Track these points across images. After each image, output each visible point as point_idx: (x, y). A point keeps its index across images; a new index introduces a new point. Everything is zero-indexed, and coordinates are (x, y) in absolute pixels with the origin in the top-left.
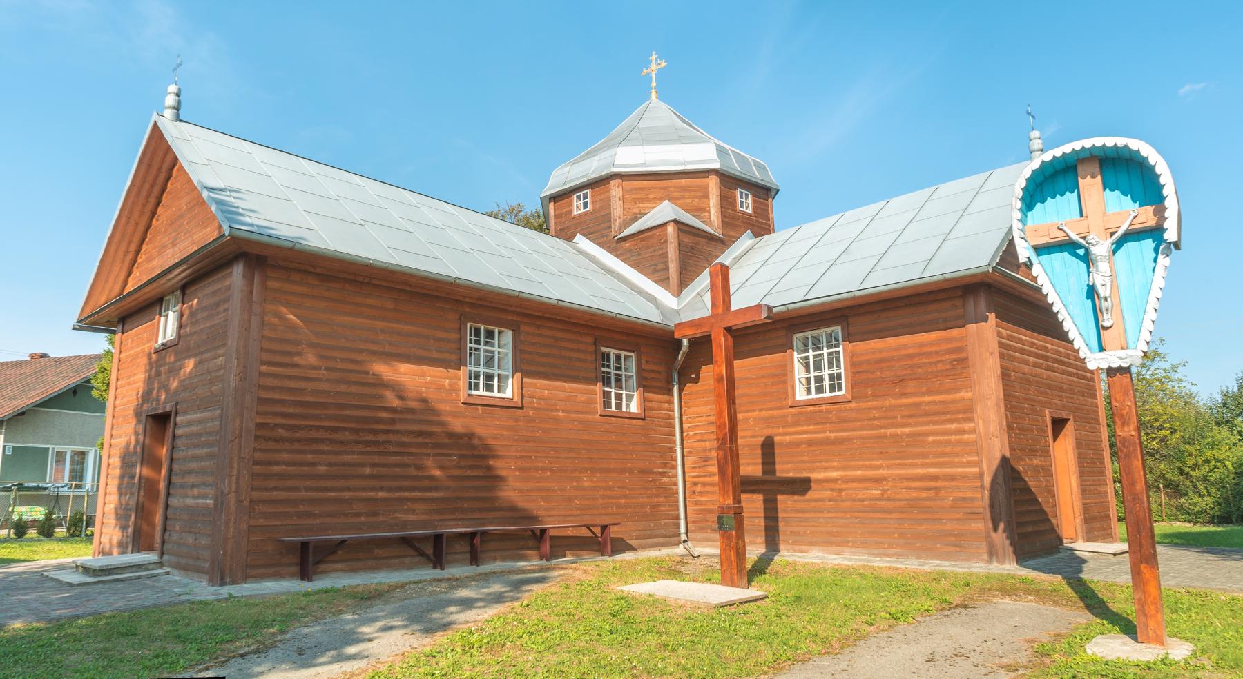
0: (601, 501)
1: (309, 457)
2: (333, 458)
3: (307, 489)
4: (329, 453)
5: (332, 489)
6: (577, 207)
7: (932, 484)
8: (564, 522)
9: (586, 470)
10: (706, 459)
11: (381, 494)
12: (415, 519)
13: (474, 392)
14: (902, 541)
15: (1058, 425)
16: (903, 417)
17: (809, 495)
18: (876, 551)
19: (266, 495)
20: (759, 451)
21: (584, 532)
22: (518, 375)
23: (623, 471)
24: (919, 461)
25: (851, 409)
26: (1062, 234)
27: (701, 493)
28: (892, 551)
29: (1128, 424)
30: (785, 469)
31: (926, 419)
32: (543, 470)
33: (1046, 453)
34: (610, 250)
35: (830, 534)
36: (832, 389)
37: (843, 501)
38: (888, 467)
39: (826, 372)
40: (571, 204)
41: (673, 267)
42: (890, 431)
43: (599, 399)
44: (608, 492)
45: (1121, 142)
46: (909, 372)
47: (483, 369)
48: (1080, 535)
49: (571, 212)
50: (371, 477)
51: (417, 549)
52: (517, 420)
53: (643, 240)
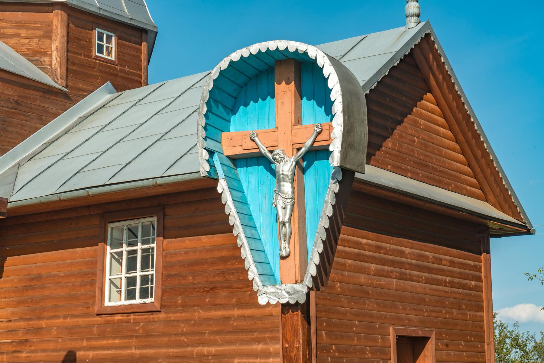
16: (212, 333)
31: (233, 337)
36: (142, 297)
39: (138, 274)
42: (196, 350)
45: (302, 47)
46: (221, 278)
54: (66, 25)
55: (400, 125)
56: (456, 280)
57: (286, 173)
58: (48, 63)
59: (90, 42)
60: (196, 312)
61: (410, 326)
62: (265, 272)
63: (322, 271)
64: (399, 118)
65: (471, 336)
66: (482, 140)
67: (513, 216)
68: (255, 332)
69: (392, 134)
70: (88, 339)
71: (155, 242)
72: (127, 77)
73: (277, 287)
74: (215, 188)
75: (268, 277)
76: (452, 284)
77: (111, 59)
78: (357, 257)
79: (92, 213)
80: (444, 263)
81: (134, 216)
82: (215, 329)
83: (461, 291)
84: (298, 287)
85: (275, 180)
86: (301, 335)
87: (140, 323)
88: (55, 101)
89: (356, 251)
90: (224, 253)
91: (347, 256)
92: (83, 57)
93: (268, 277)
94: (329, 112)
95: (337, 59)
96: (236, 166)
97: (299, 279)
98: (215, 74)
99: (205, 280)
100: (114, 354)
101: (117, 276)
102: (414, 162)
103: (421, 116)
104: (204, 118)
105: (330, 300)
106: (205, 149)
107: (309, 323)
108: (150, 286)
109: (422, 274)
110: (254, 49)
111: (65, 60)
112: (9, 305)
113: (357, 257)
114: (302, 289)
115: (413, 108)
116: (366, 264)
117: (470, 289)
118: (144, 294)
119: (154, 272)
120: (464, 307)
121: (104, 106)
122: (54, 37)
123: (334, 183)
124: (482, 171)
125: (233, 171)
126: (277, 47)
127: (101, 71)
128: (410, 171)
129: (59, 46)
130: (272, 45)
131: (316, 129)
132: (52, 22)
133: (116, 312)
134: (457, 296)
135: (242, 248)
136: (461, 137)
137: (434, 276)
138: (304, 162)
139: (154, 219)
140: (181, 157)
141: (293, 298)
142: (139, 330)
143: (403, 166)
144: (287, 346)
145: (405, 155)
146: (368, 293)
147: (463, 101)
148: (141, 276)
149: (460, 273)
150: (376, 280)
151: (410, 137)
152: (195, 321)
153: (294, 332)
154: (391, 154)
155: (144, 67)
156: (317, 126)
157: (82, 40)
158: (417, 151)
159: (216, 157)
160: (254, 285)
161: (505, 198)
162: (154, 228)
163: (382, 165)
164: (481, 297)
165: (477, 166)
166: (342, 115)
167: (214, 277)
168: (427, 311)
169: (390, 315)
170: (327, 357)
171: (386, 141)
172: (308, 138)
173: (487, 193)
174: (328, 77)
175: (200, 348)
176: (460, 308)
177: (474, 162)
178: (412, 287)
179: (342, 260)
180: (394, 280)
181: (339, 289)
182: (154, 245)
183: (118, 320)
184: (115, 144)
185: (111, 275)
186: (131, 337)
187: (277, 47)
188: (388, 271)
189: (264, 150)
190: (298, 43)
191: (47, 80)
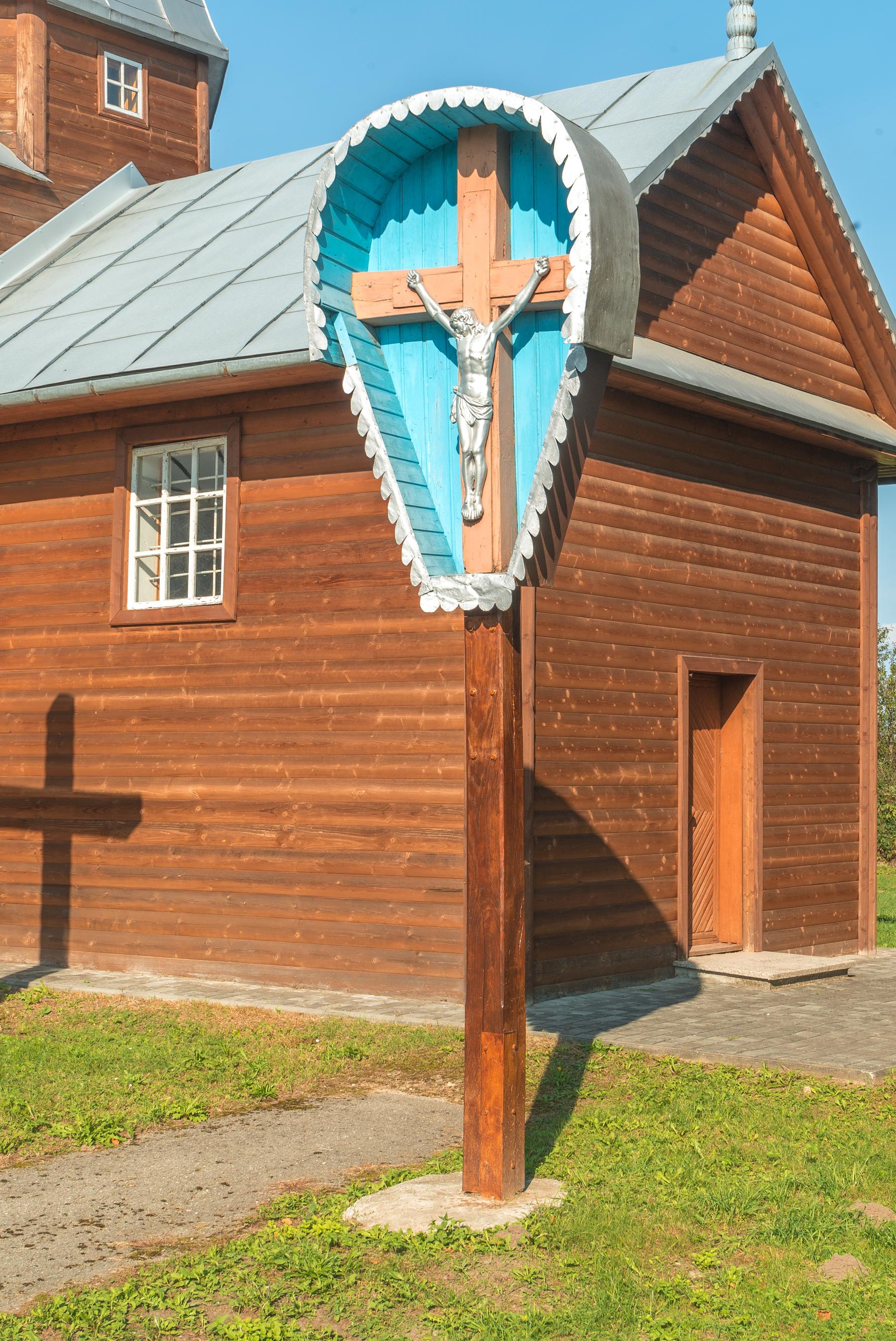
7: (375, 822)
15: (716, 694)
16: (334, 663)
17: (138, 836)
18: (256, 969)
20: (42, 728)
24: (354, 768)
26: (412, 298)
28: (288, 971)
29: (490, 736)
30: (93, 777)
31: (374, 671)
33: (665, 752)
35: (170, 928)
36: (199, 593)
37: (202, 852)
38: (297, 777)
39: (192, 547)
45: (512, 101)
46: (351, 559)
48: (750, 934)
54: (44, 43)
55: (709, 257)
56: (808, 566)
57: (476, 355)
58: (9, 123)
60: (303, 623)
61: (717, 654)
62: (435, 550)
63: (545, 549)
64: (708, 244)
65: (833, 673)
66: (870, 289)
68: (418, 662)
69: (692, 276)
70: (97, 673)
71: (225, 487)
72: (169, 153)
73: (457, 578)
74: (338, 381)
75: (440, 559)
76: (801, 574)
77: (135, 115)
78: (617, 521)
79: (100, 428)
80: (787, 532)
81: (183, 435)
82: (340, 656)
83: (817, 587)
84: (497, 579)
85: (456, 369)
86: (501, 671)
87: (196, 642)
88: (25, 202)
89: (616, 508)
90: (359, 510)
91: (598, 517)
92: (78, 112)
93: (440, 559)
94: (563, 234)
95: (583, 124)
96: (380, 340)
97: (499, 564)
98: (339, 153)
99: (322, 561)
100: (147, 701)
101: (153, 550)
102: (735, 333)
103: (751, 241)
104: (317, 244)
105: (562, 602)
106: (319, 305)
107: (517, 647)
108: (214, 571)
109: (743, 553)
110: (417, 104)
111: (43, 117)
113: (617, 521)
114: (505, 582)
115: (736, 224)
116: (635, 534)
117: (835, 583)
118: (204, 587)
119: (222, 546)
120: (822, 618)
121: (121, 212)
122: (20, 70)
123: (571, 377)
124: (869, 351)
125: (373, 350)
126: (463, 101)
127: (115, 141)
128: (725, 351)
129: (30, 89)
130: (453, 96)
131: (537, 268)
132: (15, 38)
133: (149, 621)
134: (810, 597)
135: (390, 503)
136: (829, 282)
137: (766, 558)
138: (513, 333)
139: (223, 441)
140: (275, 319)
141: (488, 601)
142: (194, 655)
143: (714, 341)
144: (475, 691)
145: (717, 319)
146: (637, 590)
147: (835, 211)
148: (198, 553)
149: (817, 553)
150: (653, 565)
151: (728, 283)
152: (301, 639)
153: (489, 665)
154: (689, 317)
155: (202, 133)
156: (540, 263)
157: (77, 76)
158: (741, 310)
159: (340, 321)
160: (413, 574)
162: (221, 456)
163: (671, 340)
164: (856, 599)
165: (859, 342)
166: (588, 240)
167: (340, 555)
168: (749, 625)
169: (678, 633)
170: (556, 711)
171: (681, 290)
172: (523, 286)
173: (877, 396)
174: (564, 163)
175: (311, 692)
176: (814, 620)
177: (852, 334)
178: (722, 578)
179: (587, 526)
180: (688, 566)
181: (581, 582)
182: (223, 493)
183: (153, 637)
184: (144, 291)
185: (138, 550)
186: (179, 669)
187: (463, 101)
188: (677, 548)
189: (435, 309)
190: (504, 92)
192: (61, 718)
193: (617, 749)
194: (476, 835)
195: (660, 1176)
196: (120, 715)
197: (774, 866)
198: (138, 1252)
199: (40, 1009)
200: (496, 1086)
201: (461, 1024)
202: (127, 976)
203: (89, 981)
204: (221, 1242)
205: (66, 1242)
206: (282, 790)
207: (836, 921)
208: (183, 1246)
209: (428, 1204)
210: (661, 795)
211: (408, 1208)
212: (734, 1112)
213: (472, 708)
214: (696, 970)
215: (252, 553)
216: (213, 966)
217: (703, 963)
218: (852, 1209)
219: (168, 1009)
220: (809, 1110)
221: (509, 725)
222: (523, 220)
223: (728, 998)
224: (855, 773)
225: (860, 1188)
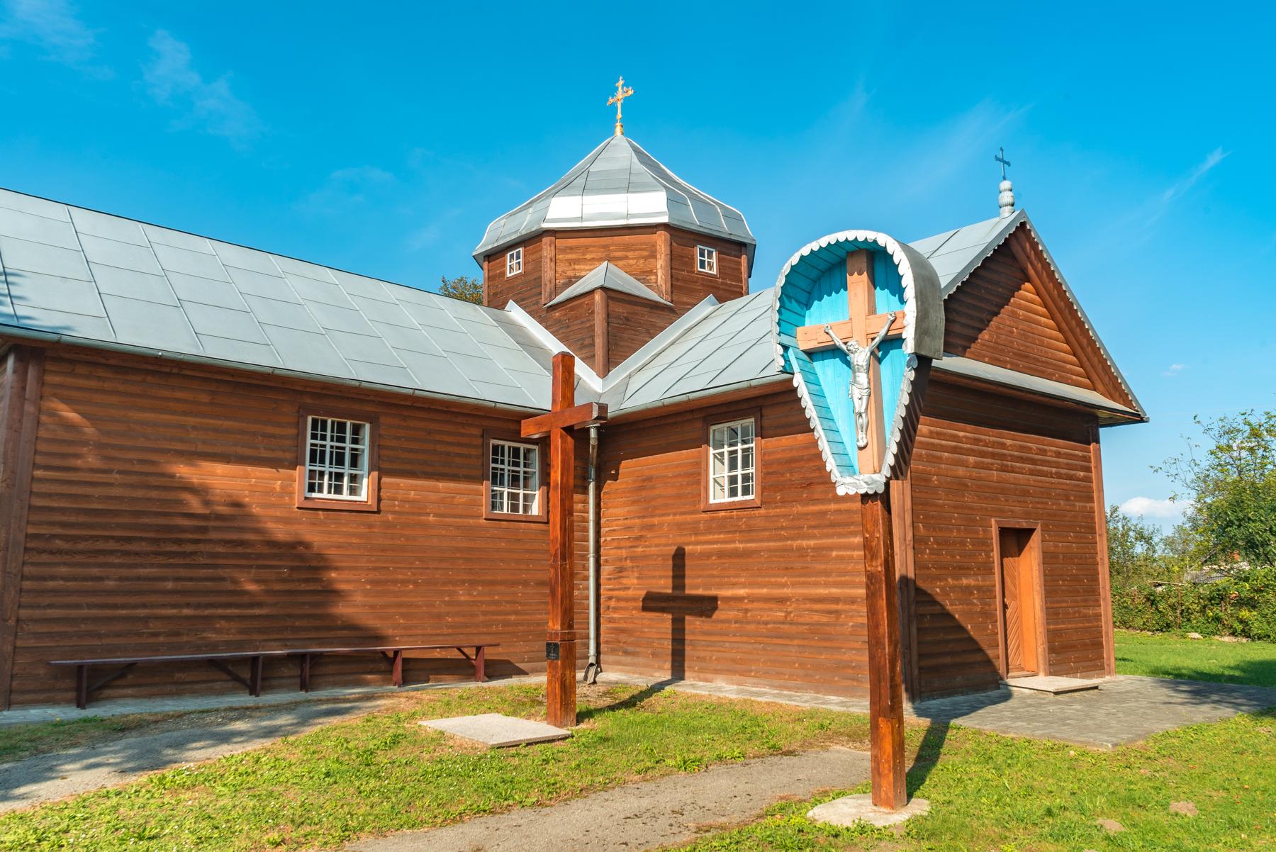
0: (481, 618)
1: (95, 571)
2: (124, 572)
3: (90, 606)
4: (121, 566)
5: (123, 606)
6: (513, 266)
7: (834, 607)
8: (429, 642)
9: (463, 582)
10: (621, 570)
11: (186, 612)
12: (223, 638)
13: (314, 495)
14: (802, 672)
15: (1014, 539)
16: (809, 527)
17: (716, 615)
18: (776, 682)
19: (38, 613)
21: (455, 654)
22: (375, 474)
23: (515, 583)
24: (822, 579)
25: (760, 516)
27: (615, 609)
28: (792, 683)
30: (695, 587)
31: (830, 531)
32: (404, 582)
34: (541, 321)
35: (734, 661)
37: (748, 623)
38: (794, 585)
39: (739, 472)
40: (504, 265)
41: (599, 341)
42: (796, 544)
43: (485, 501)
44: (493, 608)
45: (871, 235)
47: (347, 470)
48: (1042, 667)
49: (504, 273)
50: (174, 592)
51: (229, 673)
52: (370, 526)
53: (572, 309)
56: (1062, 471)
59: (692, 258)
65: (1081, 527)
67: (1125, 405)
72: (729, 288)
75: (847, 468)
76: (1059, 476)
78: (954, 450)
84: (876, 477)
93: (847, 468)
110: (823, 242)
112: (625, 504)
113: (954, 450)
114: (880, 479)
117: (1078, 479)
118: (746, 491)
130: (841, 236)
136: (1064, 325)
139: (753, 420)
143: (1002, 358)
150: (975, 473)
159: (791, 351)
161: (1115, 388)
176: (1068, 499)
177: (1079, 351)
182: (753, 445)
186: (735, 532)
191: (654, 296)
192: (679, 557)
193: (960, 568)
194: (872, 613)
195: (984, 800)
196: (707, 555)
197: (1054, 630)
198: (698, 830)
199: (669, 700)
200: (888, 747)
201: (868, 712)
202: (713, 685)
203: (694, 687)
204: (742, 825)
205: (663, 822)
206: (787, 591)
207: (1091, 660)
208: (722, 828)
209: (854, 811)
210: (987, 592)
211: (841, 813)
212: (1030, 765)
213: (867, 546)
214: (1007, 685)
215: (768, 473)
216: (755, 680)
217: (1011, 682)
218: (1097, 823)
219: (731, 702)
220: (1073, 765)
221: (886, 553)
222: (882, 295)
223: (1029, 701)
224: (1097, 580)
225: (1102, 812)
